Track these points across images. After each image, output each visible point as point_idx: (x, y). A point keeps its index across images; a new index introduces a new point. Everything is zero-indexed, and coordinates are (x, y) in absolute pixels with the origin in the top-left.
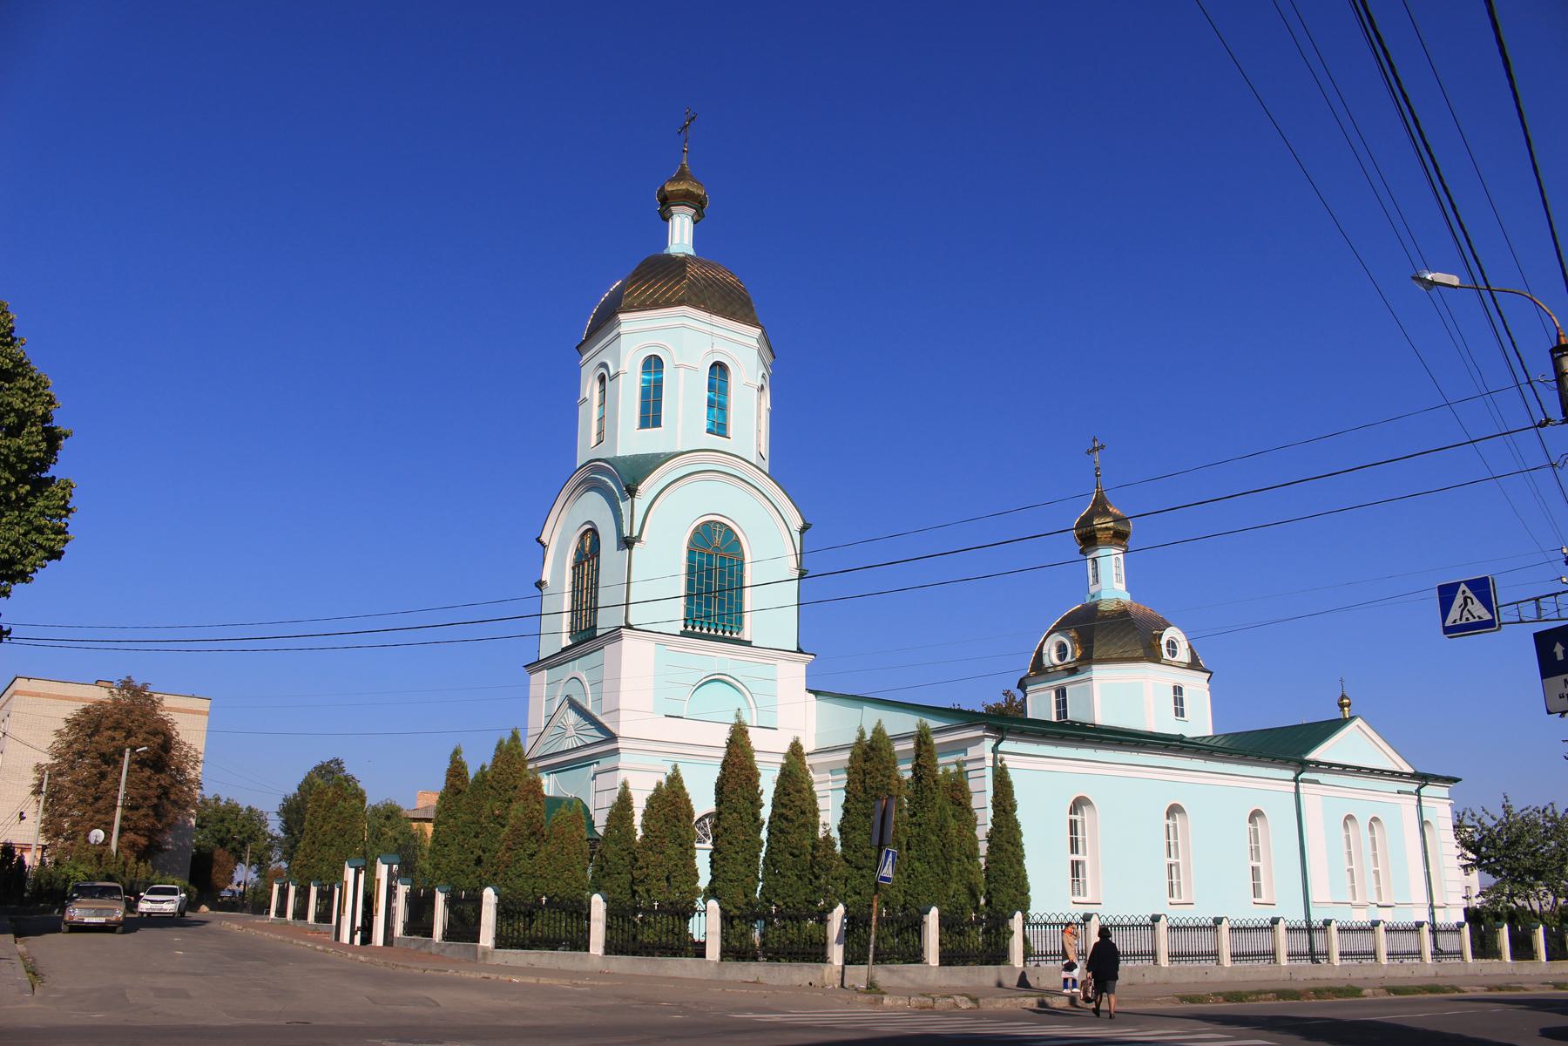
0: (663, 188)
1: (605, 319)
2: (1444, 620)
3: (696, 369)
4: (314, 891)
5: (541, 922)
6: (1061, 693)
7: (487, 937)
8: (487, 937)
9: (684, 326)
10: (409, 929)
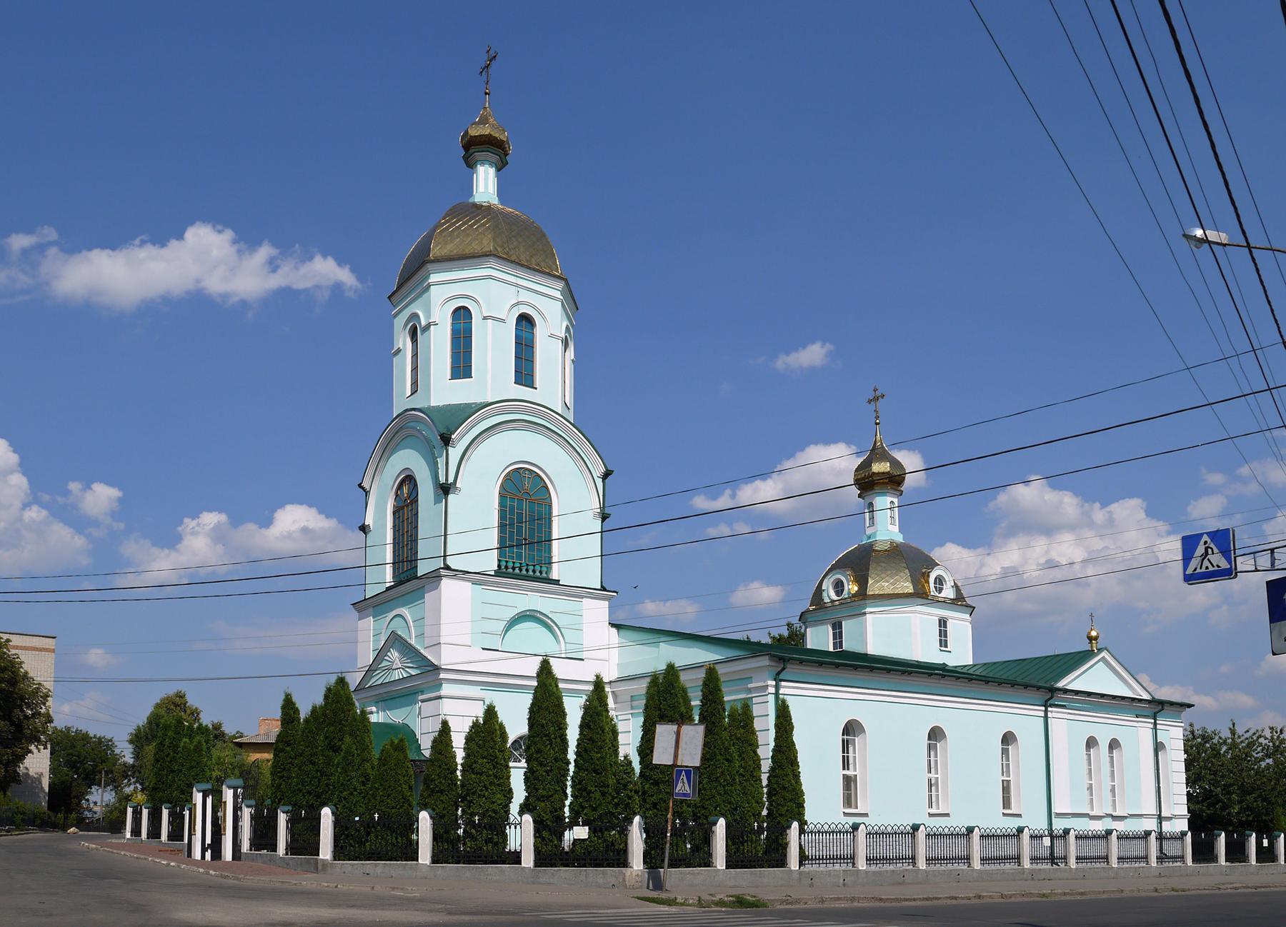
0: (466, 133)
1: (413, 274)
2: (1185, 569)
3: (503, 321)
4: (165, 813)
5: (375, 838)
7: (326, 852)
8: (326, 852)
10: (255, 844)
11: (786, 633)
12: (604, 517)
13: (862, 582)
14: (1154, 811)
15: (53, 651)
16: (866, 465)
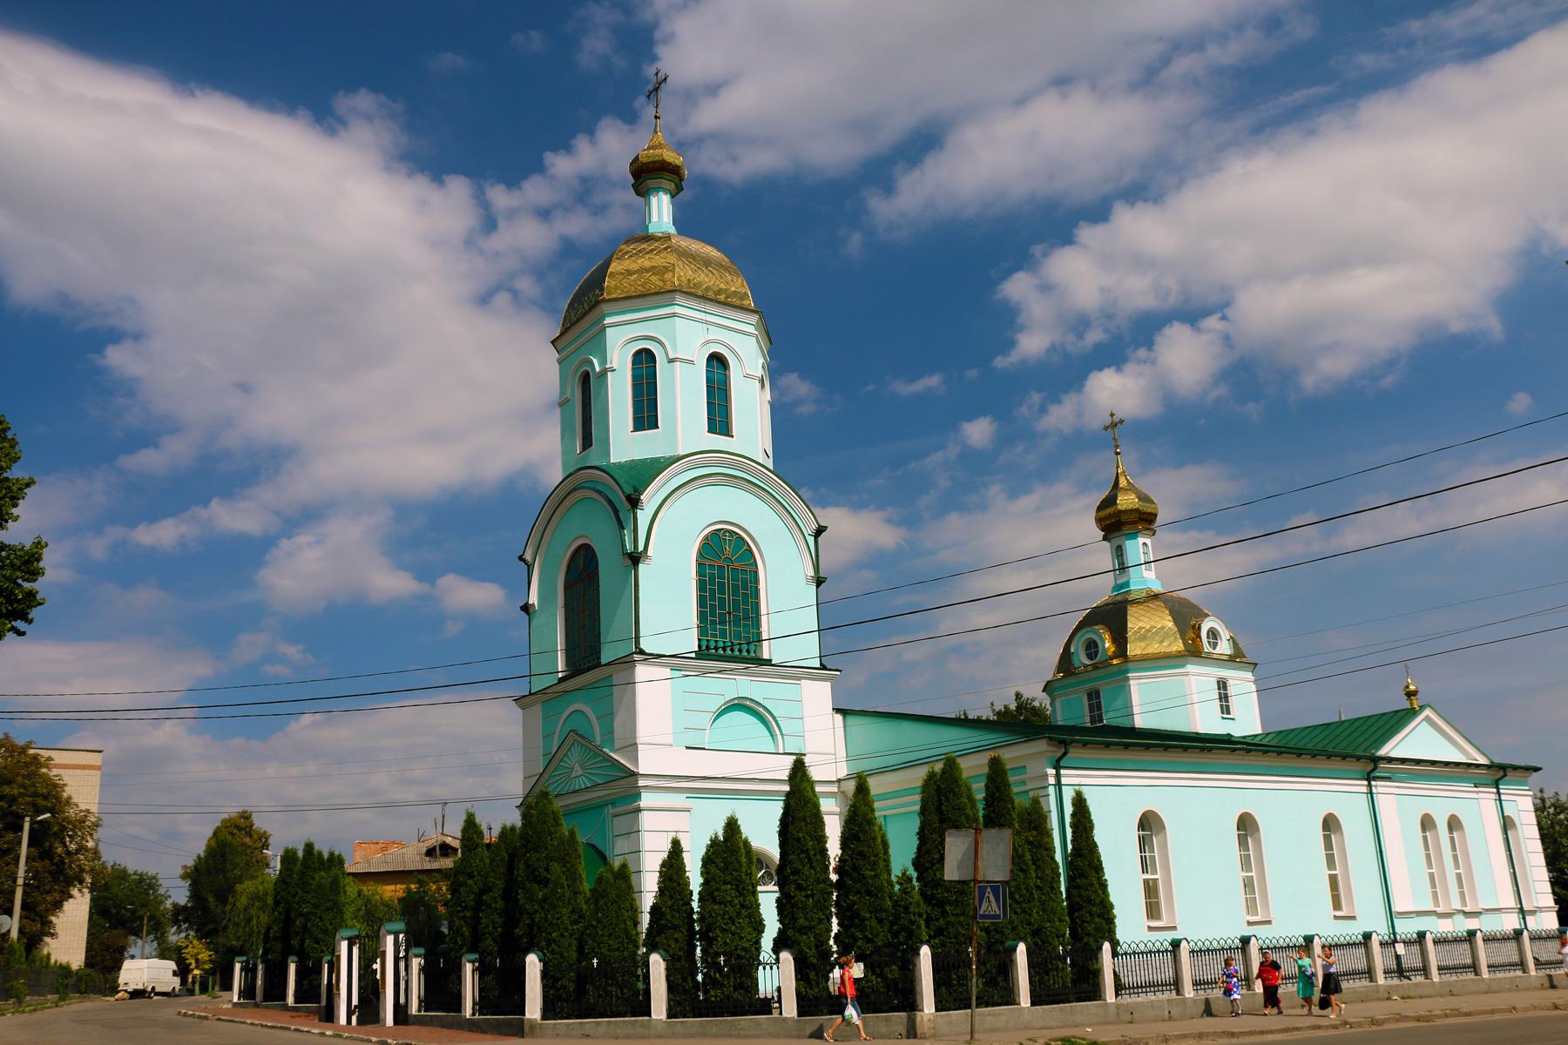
3: (692, 362)
6: (1094, 696)
9: (674, 315)
11: (1013, 707)
12: (819, 582)
13: (1120, 639)
14: (1511, 902)
15: (98, 768)
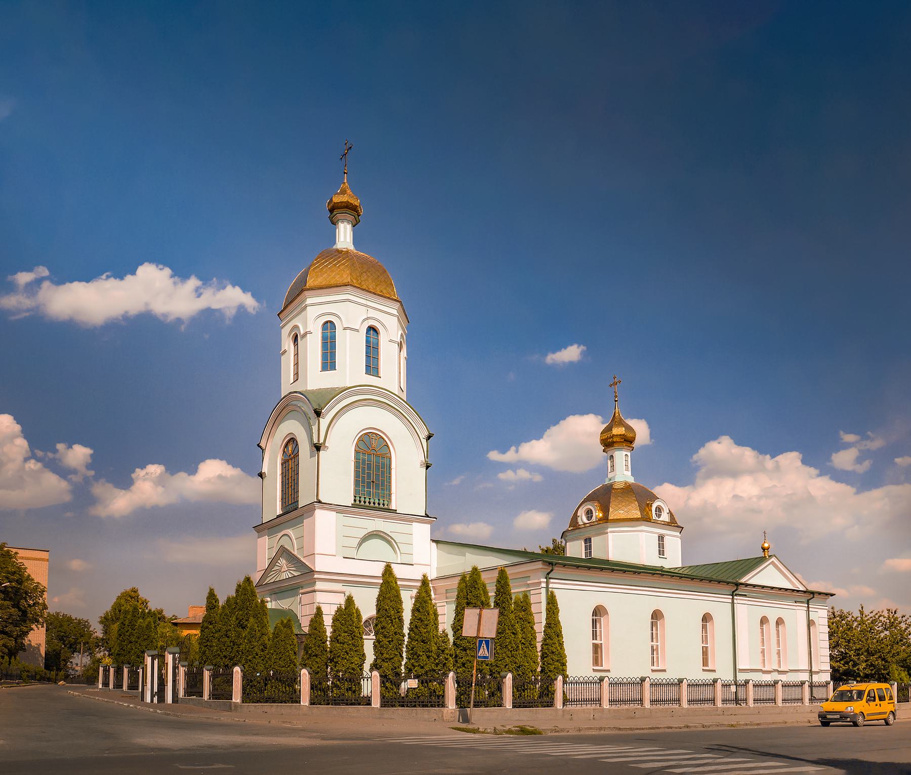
0: (331, 200)
4: (126, 671)
10: (188, 693)
11: (551, 547)
13: (605, 509)
15: (48, 560)
16: (609, 429)
